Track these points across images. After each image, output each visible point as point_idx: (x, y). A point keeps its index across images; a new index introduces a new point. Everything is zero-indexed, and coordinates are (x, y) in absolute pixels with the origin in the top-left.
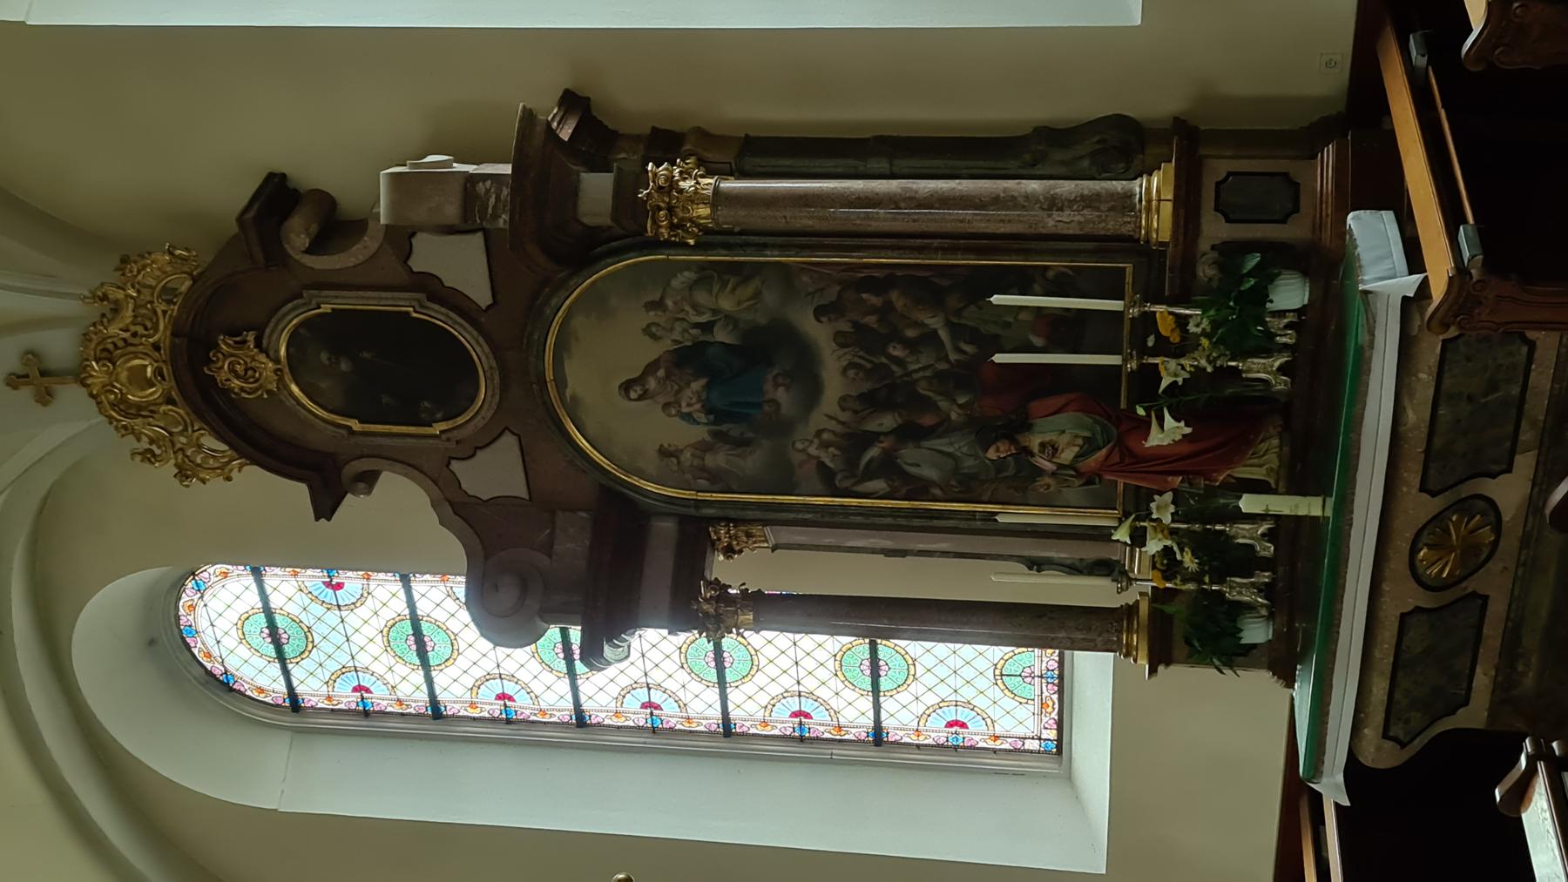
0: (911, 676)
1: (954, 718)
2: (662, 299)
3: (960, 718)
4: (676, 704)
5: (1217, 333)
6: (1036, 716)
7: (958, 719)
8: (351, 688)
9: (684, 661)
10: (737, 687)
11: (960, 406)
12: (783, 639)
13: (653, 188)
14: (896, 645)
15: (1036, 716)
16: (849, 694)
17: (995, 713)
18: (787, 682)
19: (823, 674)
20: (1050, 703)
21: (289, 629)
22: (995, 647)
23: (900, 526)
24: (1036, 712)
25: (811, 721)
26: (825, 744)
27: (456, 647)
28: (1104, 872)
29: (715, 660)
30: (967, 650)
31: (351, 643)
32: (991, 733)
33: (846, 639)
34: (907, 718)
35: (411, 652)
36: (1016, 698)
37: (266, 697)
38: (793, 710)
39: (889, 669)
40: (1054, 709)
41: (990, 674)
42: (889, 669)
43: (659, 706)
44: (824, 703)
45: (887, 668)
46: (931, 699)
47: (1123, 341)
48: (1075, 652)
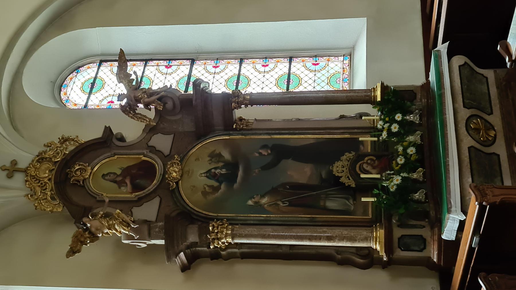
0: (277, 80)
1: (316, 66)
2: (47, 197)
3: (314, 66)
4: (306, 66)
5: (316, 193)
6: (341, 69)
7: (315, 66)
8: (319, 65)
9: (328, 82)
10: (336, 72)
11: (180, 165)
12: (267, 90)
13: (221, 246)
14: (229, 91)
15: (341, 69)
16: (298, 72)
17: (303, 69)
18: (319, 75)
19: (306, 79)
20: (69, 79)
21: (339, 85)
22: (327, 90)
23: (278, 130)
24: (341, 68)
25: (213, 65)
26: (230, 58)
27: (300, 82)
28: (366, 18)
29: (290, 82)
30: (310, 89)
31: (315, 83)
32: (254, 64)
33: (297, 90)
34: (280, 66)
35: (292, 79)
36: (295, 74)
37: (86, 67)
38: (318, 66)
39: (293, 82)
40: (347, 71)
41: (303, 82)
42: (293, 82)
43: (313, 65)
44: (208, 72)
45: (242, 82)
46: (323, 72)
47: (321, 190)
48: (366, 89)
